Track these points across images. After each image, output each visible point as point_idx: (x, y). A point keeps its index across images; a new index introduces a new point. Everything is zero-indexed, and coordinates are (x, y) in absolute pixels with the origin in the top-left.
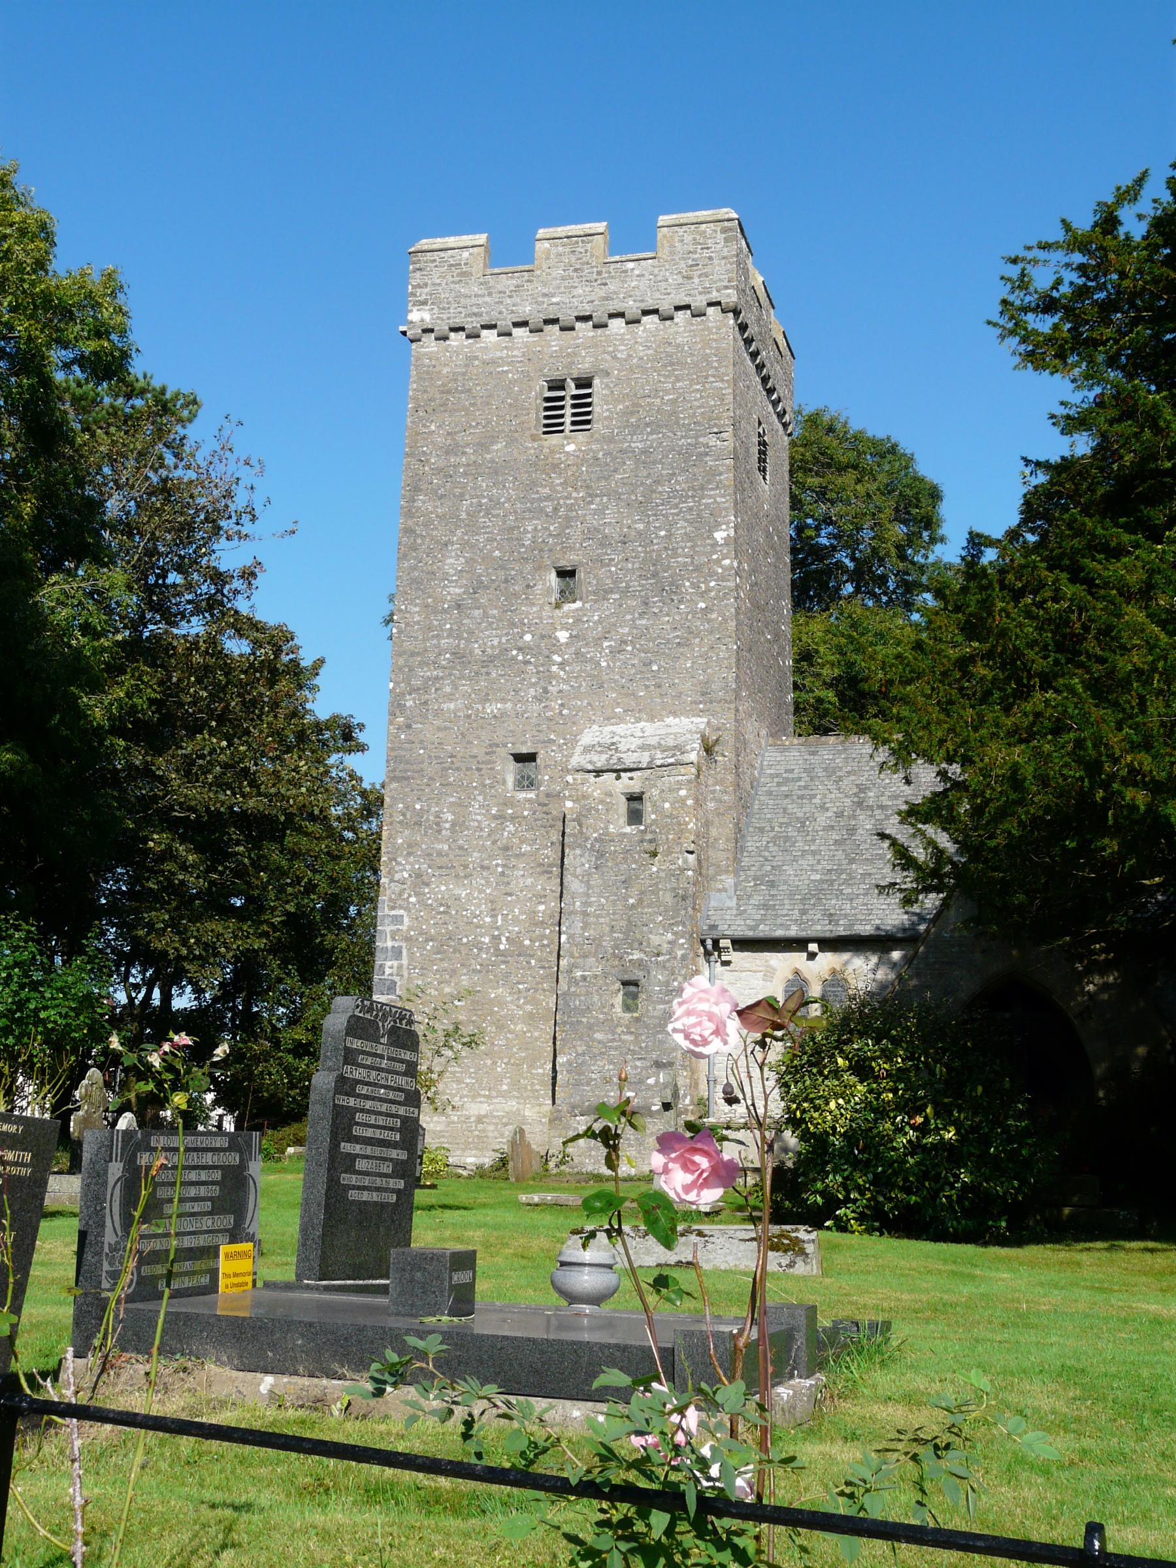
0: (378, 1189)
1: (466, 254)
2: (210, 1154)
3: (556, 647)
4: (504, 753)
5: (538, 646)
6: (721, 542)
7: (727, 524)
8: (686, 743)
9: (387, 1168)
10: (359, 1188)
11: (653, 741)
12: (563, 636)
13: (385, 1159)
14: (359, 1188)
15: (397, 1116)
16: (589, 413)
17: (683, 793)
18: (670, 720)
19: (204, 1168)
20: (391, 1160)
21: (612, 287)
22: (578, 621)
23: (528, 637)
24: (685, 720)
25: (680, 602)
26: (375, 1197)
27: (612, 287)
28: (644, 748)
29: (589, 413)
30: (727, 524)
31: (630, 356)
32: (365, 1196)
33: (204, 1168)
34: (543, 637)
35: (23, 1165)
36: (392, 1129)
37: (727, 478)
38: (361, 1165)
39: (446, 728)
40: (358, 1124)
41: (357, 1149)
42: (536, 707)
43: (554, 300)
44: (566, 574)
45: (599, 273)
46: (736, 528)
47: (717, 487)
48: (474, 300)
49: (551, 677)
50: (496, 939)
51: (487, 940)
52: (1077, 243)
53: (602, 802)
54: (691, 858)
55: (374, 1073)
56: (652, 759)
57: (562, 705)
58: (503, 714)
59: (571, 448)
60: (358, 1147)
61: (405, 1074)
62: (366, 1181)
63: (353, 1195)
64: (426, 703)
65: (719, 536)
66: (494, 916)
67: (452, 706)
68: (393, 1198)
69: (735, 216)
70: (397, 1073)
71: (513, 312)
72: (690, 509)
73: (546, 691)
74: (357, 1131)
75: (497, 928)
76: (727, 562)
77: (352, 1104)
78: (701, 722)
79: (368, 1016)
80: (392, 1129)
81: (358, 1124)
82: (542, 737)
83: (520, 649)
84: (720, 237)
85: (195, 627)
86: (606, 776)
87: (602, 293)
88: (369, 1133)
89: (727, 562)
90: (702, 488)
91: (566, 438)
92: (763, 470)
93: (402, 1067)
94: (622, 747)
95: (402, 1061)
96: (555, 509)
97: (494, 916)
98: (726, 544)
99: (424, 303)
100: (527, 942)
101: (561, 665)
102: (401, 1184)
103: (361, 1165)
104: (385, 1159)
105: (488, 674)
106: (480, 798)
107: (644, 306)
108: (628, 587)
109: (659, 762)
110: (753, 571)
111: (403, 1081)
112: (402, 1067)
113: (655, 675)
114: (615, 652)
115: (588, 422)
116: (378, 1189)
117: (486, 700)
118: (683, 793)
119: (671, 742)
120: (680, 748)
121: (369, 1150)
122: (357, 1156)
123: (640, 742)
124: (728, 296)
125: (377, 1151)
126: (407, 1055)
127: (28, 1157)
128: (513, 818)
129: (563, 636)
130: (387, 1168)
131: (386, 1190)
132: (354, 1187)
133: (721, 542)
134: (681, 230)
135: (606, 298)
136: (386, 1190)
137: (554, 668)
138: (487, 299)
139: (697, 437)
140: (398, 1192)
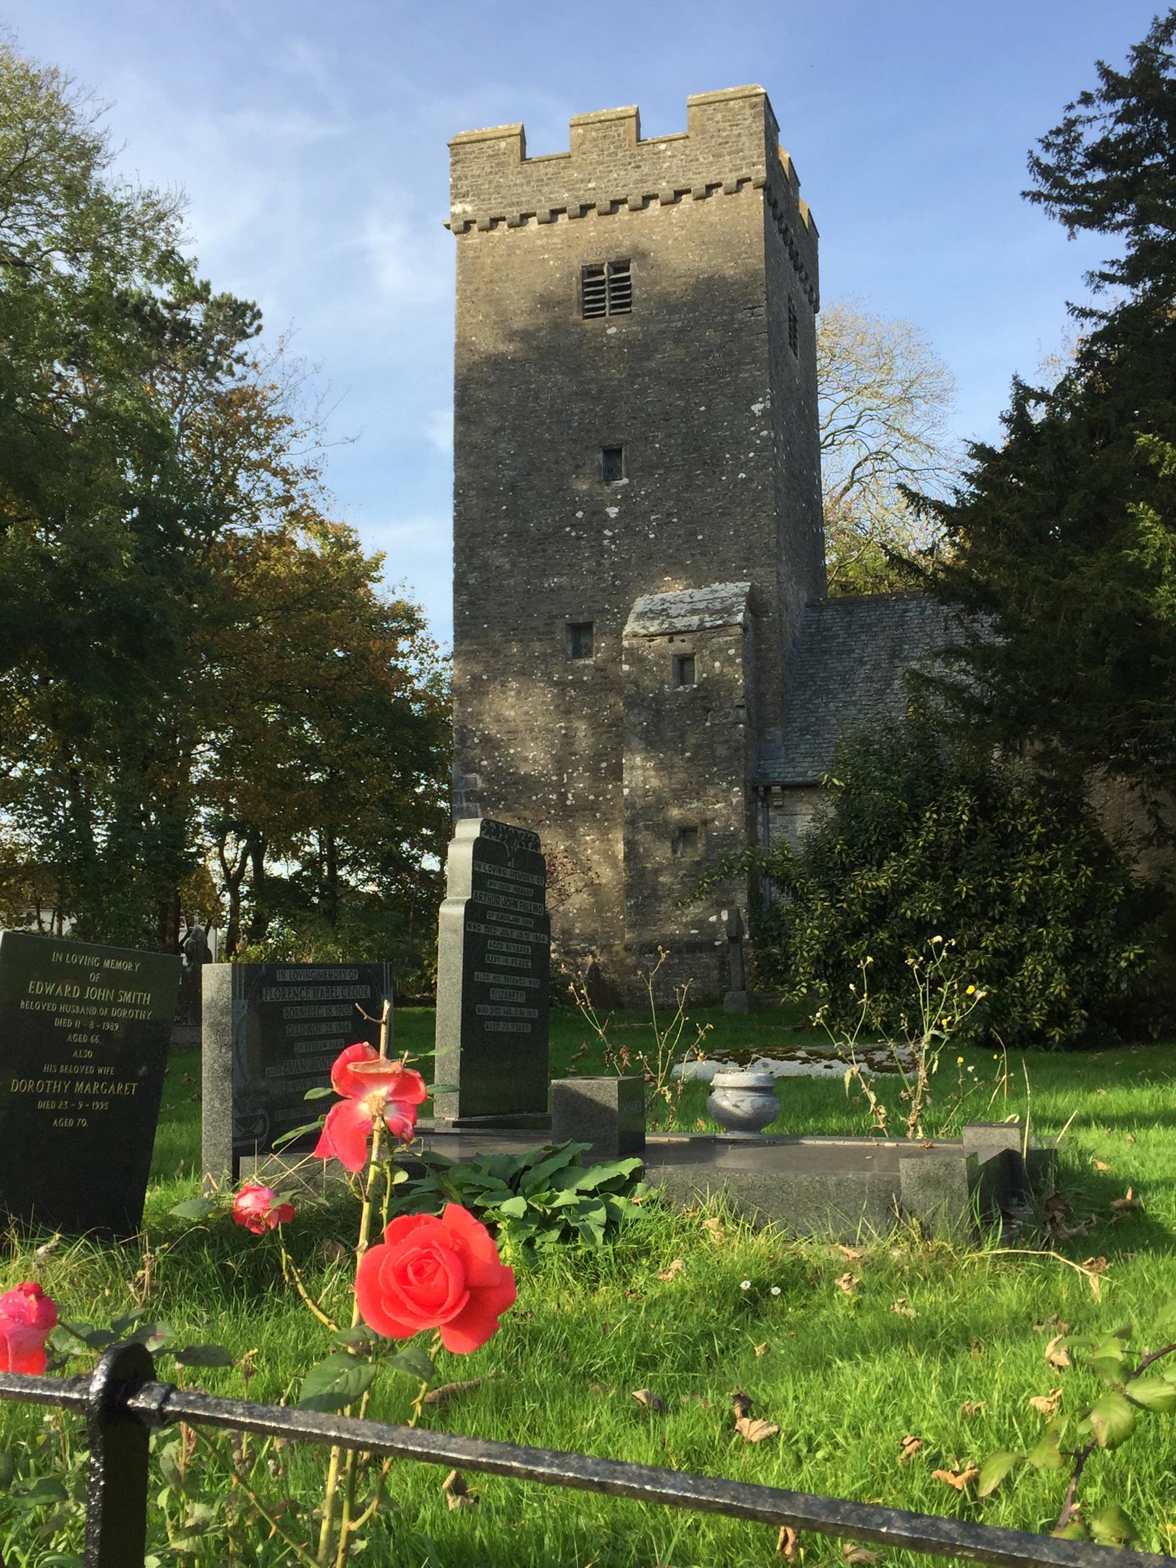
0: (514, 1020)
1: (503, 144)
2: (339, 989)
3: (606, 521)
4: (560, 624)
5: (590, 523)
6: (758, 414)
7: (764, 397)
8: (732, 606)
9: (521, 998)
10: (497, 1019)
11: (702, 605)
12: (613, 512)
13: (519, 988)
14: (497, 1019)
15: (529, 943)
16: (628, 296)
17: (732, 652)
18: (716, 586)
19: (334, 1002)
20: (525, 988)
21: (645, 170)
22: (626, 497)
23: (580, 514)
24: (731, 586)
25: (722, 474)
26: (511, 1027)
27: (645, 170)
28: (694, 612)
29: (628, 296)
30: (764, 397)
31: (665, 237)
32: (502, 1027)
33: (334, 1002)
34: (594, 513)
35: (142, 1007)
36: (523, 956)
37: (764, 352)
38: (495, 995)
39: (507, 603)
40: (490, 951)
41: (491, 978)
42: (590, 580)
43: (590, 186)
44: (612, 453)
45: (632, 156)
46: (772, 400)
47: (754, 361)
48: (515, 190)
49: (602, 551)
50: (563, 797)
51: (554, 797)
52: (1115, 86)
53: (656, 664)
54: (742, 712)
55: (502, 898)
56: (702, 621)
57: (614, 576)
58: (560, 588)
59: (612, 331)
60: (491, 976)
61: (533, 899)
62: (502, 1011)
63: (490, 1026)
64: (488, 580)
65: (757, 408)
66: (560, 775)
67: (512, 582)
68: (528, 1029)
69: (762, 90)
70: (525, 898)
71: (551, 200)
72: (728, 384)
73: (599, 564)
74: (489, 959)
75: (564, 786)
76: (765, 433)
77: (482, 931)
78: (745, 586)
79: (494, 839)
80: (523, 956)
81: (490, 951)
82: (597, 607)
83: (573, 526)
84: (748, 112)
85: (269, 522)
86: (658, 640)
87: (636, 175)
88: (501, 961)
89: (765, 433)
90: (739, 363)
91: (607, 321)
92: (794, 346)
93: (530, 892)
94: (673, 612)
95: (530, 886)
96: (600, 391)
97: (560, 775)
98: (762, 416)
99: (465, 195)
100: (592, 797)
101: (612, 539)
102: (535, 1013)
103: (495, 995)
104: (519, 988)
105: (544, 551)
106: (543, 667)
107: (677, 187)
108: (671, 461)
109: (708, 625)
110: (787, 442)
111: (530, 905)
112: (530, 892)
113: (701, 544)
114: (661, 526)
115: (628, 305)
116: (514, 1020)
117: (544, 574)
118: (732, 652)
119: (718, 605)
120: (728, 611)
121: (502, 979)
122: (491, 985)
123: (689, 607)
124: (758, 171)
125: (511, 980)
126: (534, 880)
127: (148, 998)
128: (573, 684)
129: (613, 512)
130: (521, 998)
131: (520, 1020)
132: (490, 1018)
133: (758, 414)
134: (710, 110)
135: (642, 181)
136: (520, 1020)
137: (606, 542)
138: (526, 188)
139: (732, 314)
140: (532, 1021)
